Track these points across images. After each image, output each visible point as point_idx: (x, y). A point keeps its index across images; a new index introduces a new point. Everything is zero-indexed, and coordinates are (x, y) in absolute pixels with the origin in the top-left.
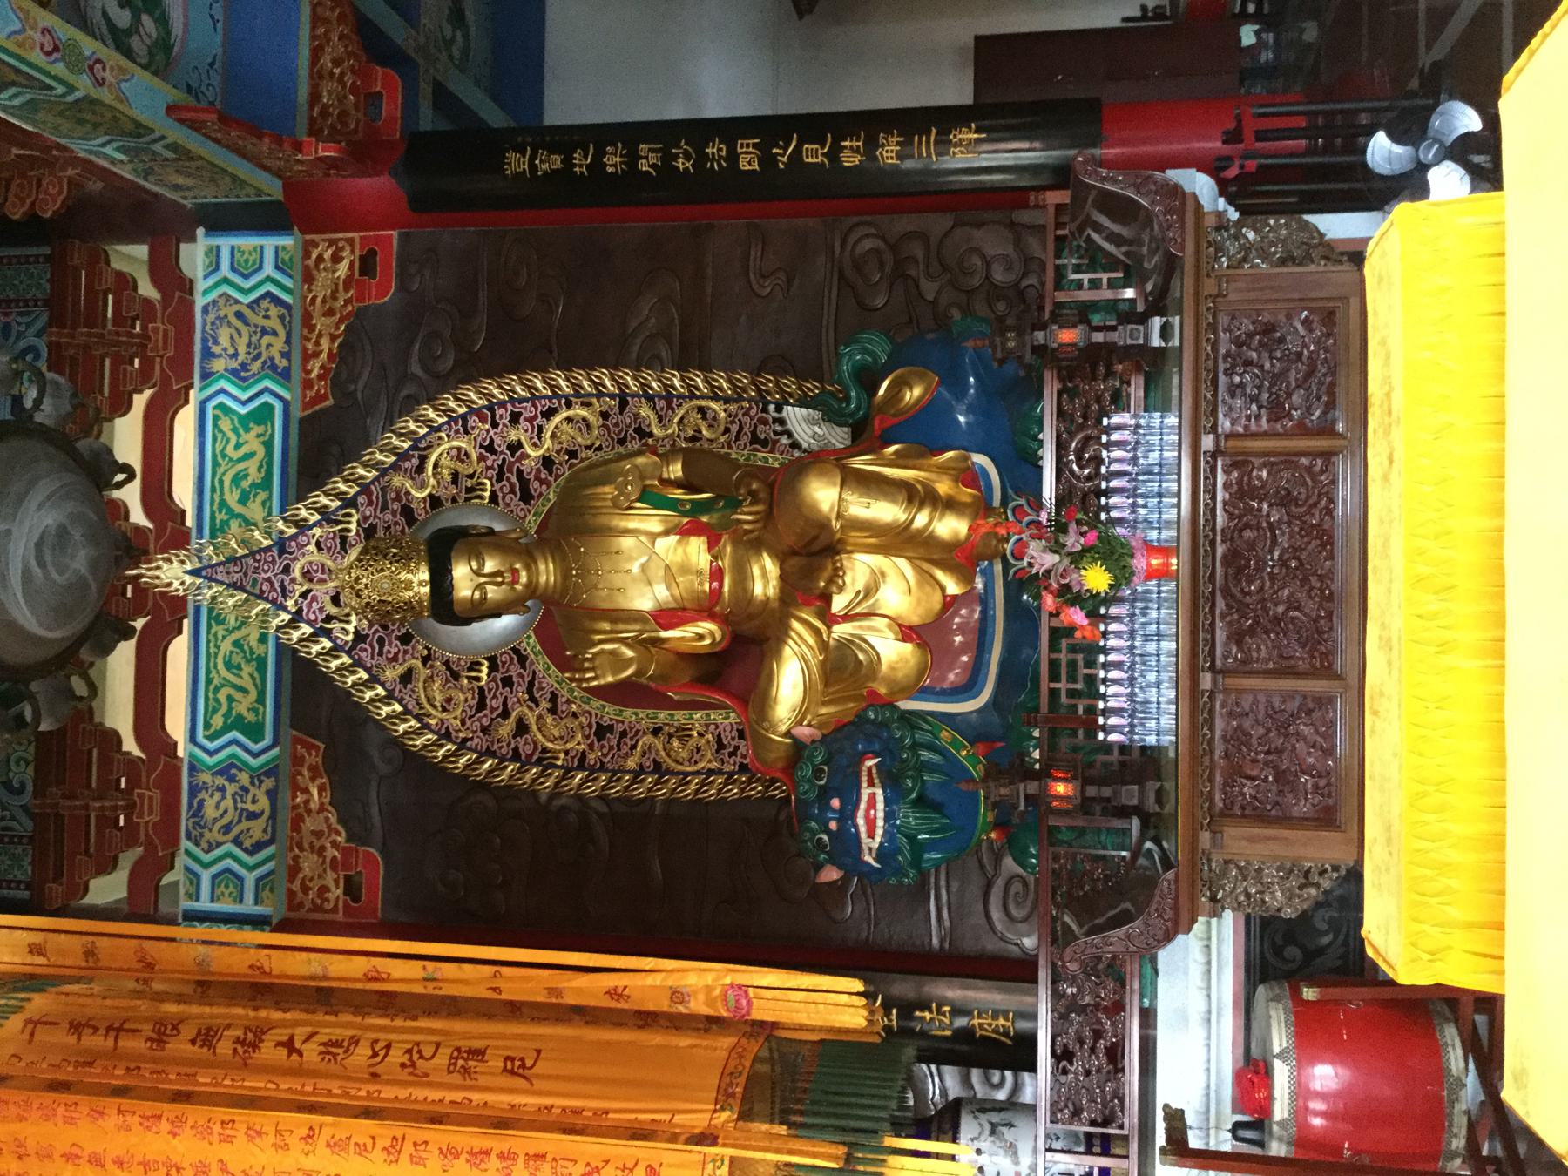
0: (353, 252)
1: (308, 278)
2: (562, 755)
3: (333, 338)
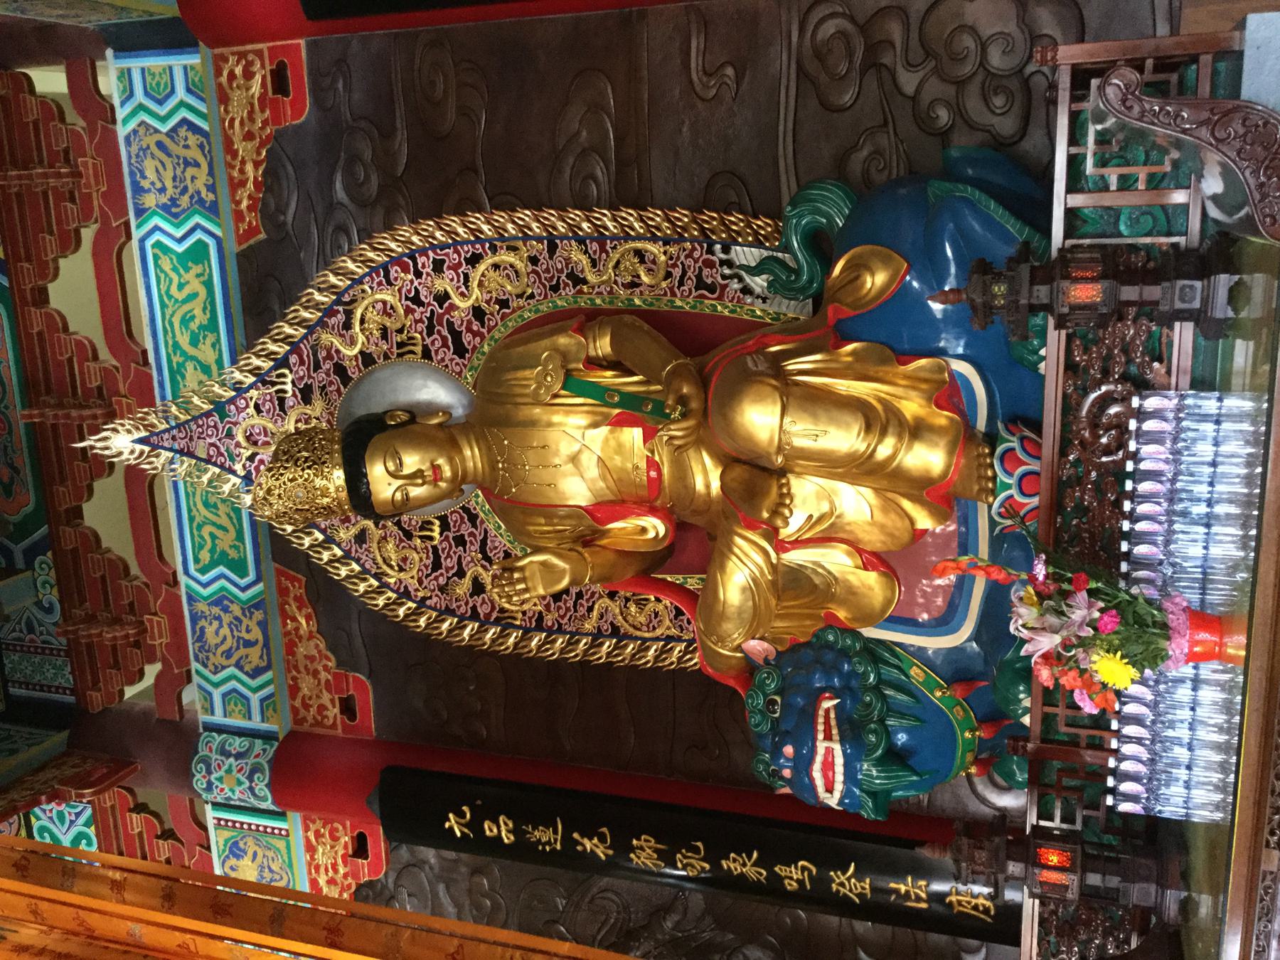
0: (263, 66)
1: (224, 99)
2: (520, 615)
3: (257, 165)
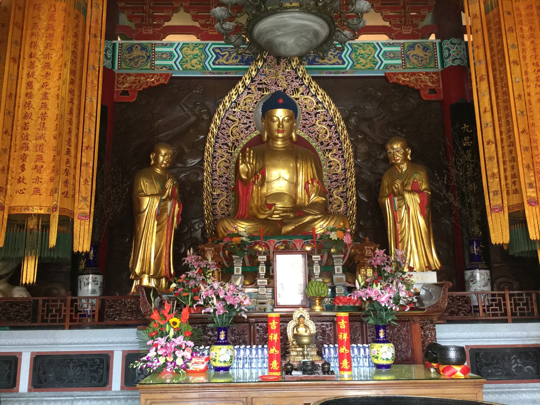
3: (409, 82)
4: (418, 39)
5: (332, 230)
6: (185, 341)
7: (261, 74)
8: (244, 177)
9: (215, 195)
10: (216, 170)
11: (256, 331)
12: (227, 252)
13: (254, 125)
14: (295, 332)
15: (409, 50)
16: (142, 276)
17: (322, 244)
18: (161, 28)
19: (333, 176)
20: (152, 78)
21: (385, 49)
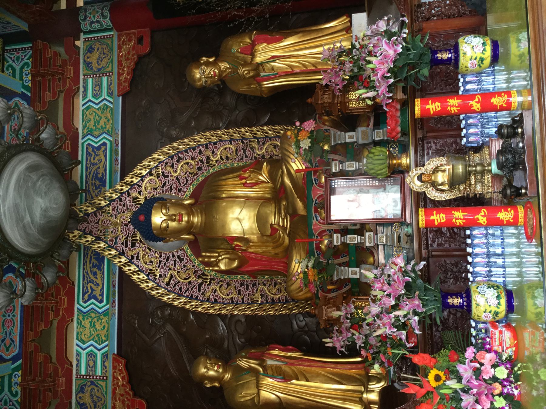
3: (128, 67)
4: (79, 59)
5: (298, 147)
6: (467, 361)
7: (115, 244)
8: (235, 264)
9: (259, 301)
10: (232, 298)
11: (441, 248)
12: (330, 287)
13: (177, 252)
14: (446, 187)
15: (92, 69)
16: (366, 401)
17: (318, 163)
18: (59, 367)
19: (239, 154)
20: (118, 379)
21: (90, 97)
